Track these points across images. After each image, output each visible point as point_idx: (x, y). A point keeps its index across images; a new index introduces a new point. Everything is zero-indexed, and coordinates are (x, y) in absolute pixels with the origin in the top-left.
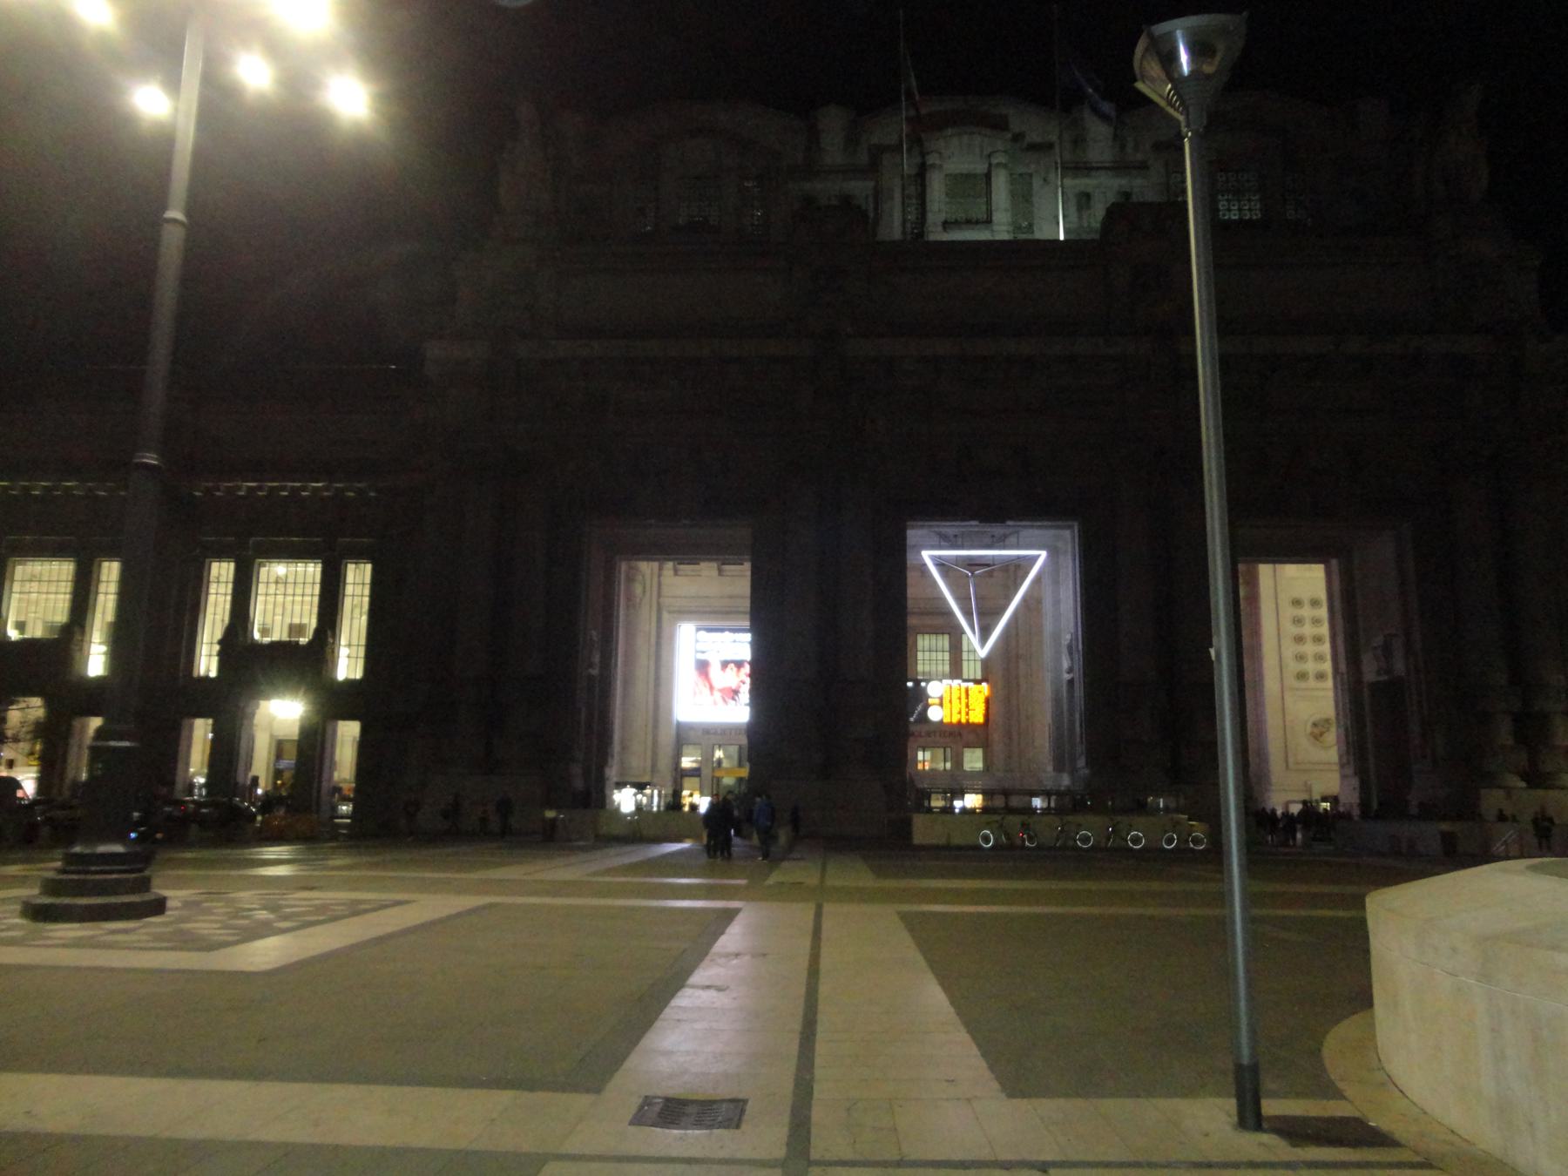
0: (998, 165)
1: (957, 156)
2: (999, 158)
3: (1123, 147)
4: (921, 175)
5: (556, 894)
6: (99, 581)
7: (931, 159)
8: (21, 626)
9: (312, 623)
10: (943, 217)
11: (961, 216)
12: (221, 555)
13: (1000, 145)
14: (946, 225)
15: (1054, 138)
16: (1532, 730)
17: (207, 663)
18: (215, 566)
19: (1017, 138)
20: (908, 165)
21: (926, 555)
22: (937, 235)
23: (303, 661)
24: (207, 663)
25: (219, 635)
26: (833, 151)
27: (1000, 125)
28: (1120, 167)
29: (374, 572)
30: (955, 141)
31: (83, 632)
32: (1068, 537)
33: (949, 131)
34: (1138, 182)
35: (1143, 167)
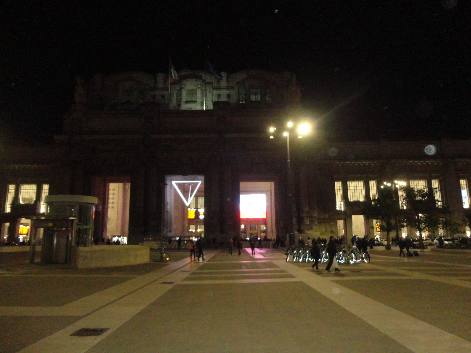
0: (199, 88)
1: (189, 85)
2: (199, 86)
3: (229, 83)
4: (181, 89)
5: (249, 276)
6: (9, 189)
7: (183, 86)
8: (23, 201)
9: (34, 199)
10: (185, 100)
11: (190, 100)
12: (12, 183)
13: (199, 83)
14: (187, 102)
15: (213, 81)
16: (300, 221)
17: (8, 210)
18: (44, 185)
19: (203, 81)
20: (178, 88)
21: (174, 183)
22: (185, 107)
23: (29, 210)
24: (8, 210)
25: (11, 203)
26: (160, 84)
27: (198, 78)
28: (227, 88)
29: (131, 185)
30: (189, 82)
31: (39, 202)
32: (168, 178)
33: (187, 79)
34: (232, 92)
35: (233, 88)
